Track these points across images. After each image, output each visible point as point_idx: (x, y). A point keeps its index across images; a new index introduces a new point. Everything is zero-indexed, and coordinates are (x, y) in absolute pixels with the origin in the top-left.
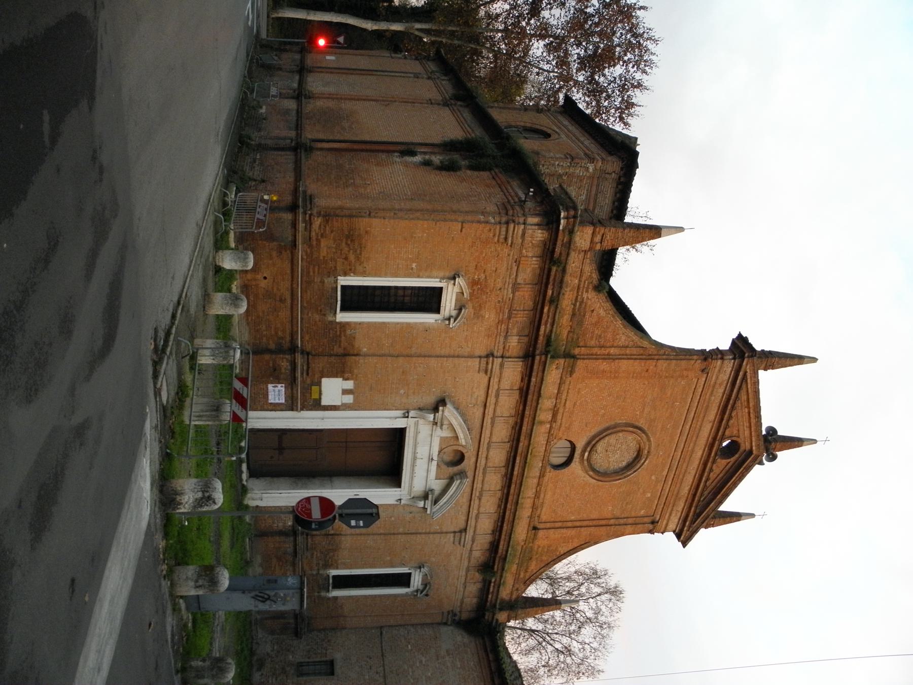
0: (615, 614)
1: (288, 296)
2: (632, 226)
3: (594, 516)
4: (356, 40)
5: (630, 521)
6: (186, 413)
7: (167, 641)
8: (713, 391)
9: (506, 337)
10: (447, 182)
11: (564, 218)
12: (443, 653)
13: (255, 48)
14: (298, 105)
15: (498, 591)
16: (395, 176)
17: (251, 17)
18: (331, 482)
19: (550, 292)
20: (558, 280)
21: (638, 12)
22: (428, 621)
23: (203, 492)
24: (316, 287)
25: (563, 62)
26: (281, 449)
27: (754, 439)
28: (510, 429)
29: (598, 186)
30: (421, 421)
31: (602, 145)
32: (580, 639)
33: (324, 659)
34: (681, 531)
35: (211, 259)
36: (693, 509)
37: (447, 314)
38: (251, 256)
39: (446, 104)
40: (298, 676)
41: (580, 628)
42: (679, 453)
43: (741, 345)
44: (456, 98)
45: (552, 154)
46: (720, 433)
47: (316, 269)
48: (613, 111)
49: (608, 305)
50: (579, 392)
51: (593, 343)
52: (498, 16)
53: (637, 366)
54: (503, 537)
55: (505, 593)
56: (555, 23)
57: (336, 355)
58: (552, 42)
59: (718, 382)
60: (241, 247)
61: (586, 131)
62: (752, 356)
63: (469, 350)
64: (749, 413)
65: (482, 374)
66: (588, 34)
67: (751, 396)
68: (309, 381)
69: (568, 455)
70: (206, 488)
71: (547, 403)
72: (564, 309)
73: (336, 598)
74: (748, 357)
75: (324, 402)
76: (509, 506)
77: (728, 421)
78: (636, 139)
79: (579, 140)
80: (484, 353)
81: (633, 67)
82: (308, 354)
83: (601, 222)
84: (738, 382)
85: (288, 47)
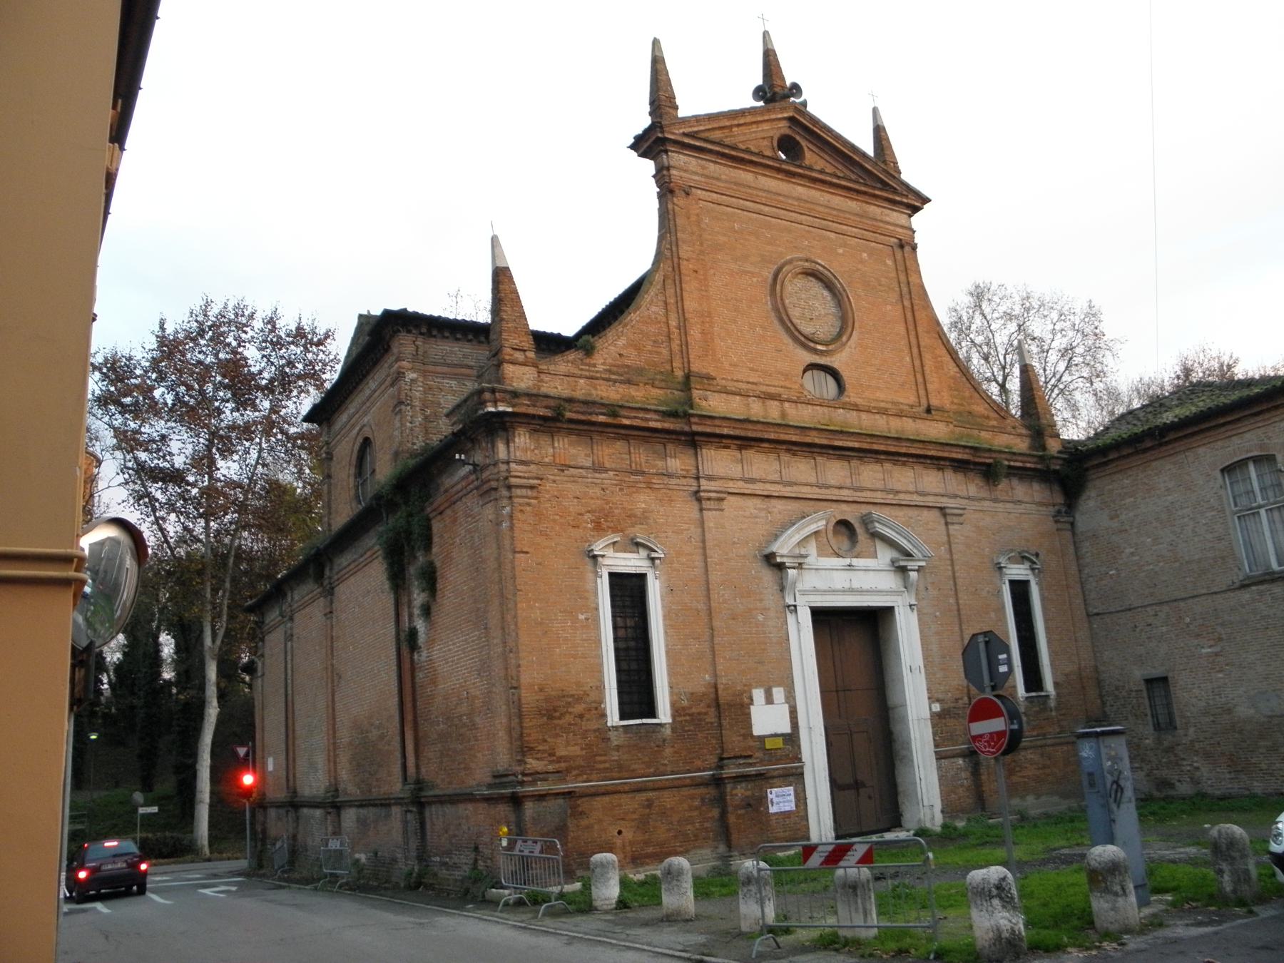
0: (1008, 293)
1: (642, 796)
2: (496, 310)
3: (901, 329)
4: (240, 729)
5: (902, 278)
6: (864, 934)
7: (1216, 933)
8: (713, 178)
9: (670, 476)
10: (454, 580)
11: (496, 406)
12: (1115, 524)
13: (264, 875)
14: (350, 806)
15: (1020, 454)
16: (451, 658)
17: (223, 888)
18: (895, 707)
19: (602, 418)
20: (583, 408)
21: (168, 332)
22: (1071, 549)
23: (991, 897)
24: (625, 757)
25: (246, 431)
26: (857, 785)
27: (773, 116)
28: (796, 458)
29: (435, 364)
30: (799, 586)
31: (376, 363)
32: (1048, 337)
33: (1145, 694)
34: (909, 206)
35: (609, 917)
36: (877, 192)
37: (646, 563)
38: (598, 857)
39: (330, 592)
40: (1175, 728)
41: (1034, 339)
42: (804, 218)
43: (647, 144)
44: (319, 577)
45: (396, 433)
46: (770, 163)
47: (598, 758)
48: (310, 356)
49: (611, 334)
50: (736, 365)
51: (665, 352)
52: (185, 528)
53: (690, 286)
54: (946, 455)
55: (1022, 445)
56: (190, 447)
57: (719, 717)
58: (218, 449)
59: (700, 170)
60: (579, 873)
61: (355, 388)
62: (661, 127)
63: (692, 527)
64: (739, 125)
65: (725, 504)
66: (204, 400)
67: (716, 125)
68: (759, 754)
69: (823, 374)
70: (985, 893)
71: (756, 410)
72: (628, 396)
73: (1056, 685)
74: (662, 132)
75: (786, 729)
76: (903, 450)
77: (752, 153)
78: (361, 316)
79: (370, 396)
80: (695, 505)
81: (246, 332)
82: (722, 759)
83: (497, 353)
84: (698, 144)
85: (259, 828)
